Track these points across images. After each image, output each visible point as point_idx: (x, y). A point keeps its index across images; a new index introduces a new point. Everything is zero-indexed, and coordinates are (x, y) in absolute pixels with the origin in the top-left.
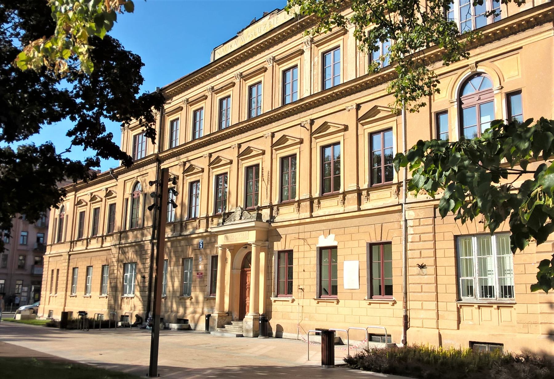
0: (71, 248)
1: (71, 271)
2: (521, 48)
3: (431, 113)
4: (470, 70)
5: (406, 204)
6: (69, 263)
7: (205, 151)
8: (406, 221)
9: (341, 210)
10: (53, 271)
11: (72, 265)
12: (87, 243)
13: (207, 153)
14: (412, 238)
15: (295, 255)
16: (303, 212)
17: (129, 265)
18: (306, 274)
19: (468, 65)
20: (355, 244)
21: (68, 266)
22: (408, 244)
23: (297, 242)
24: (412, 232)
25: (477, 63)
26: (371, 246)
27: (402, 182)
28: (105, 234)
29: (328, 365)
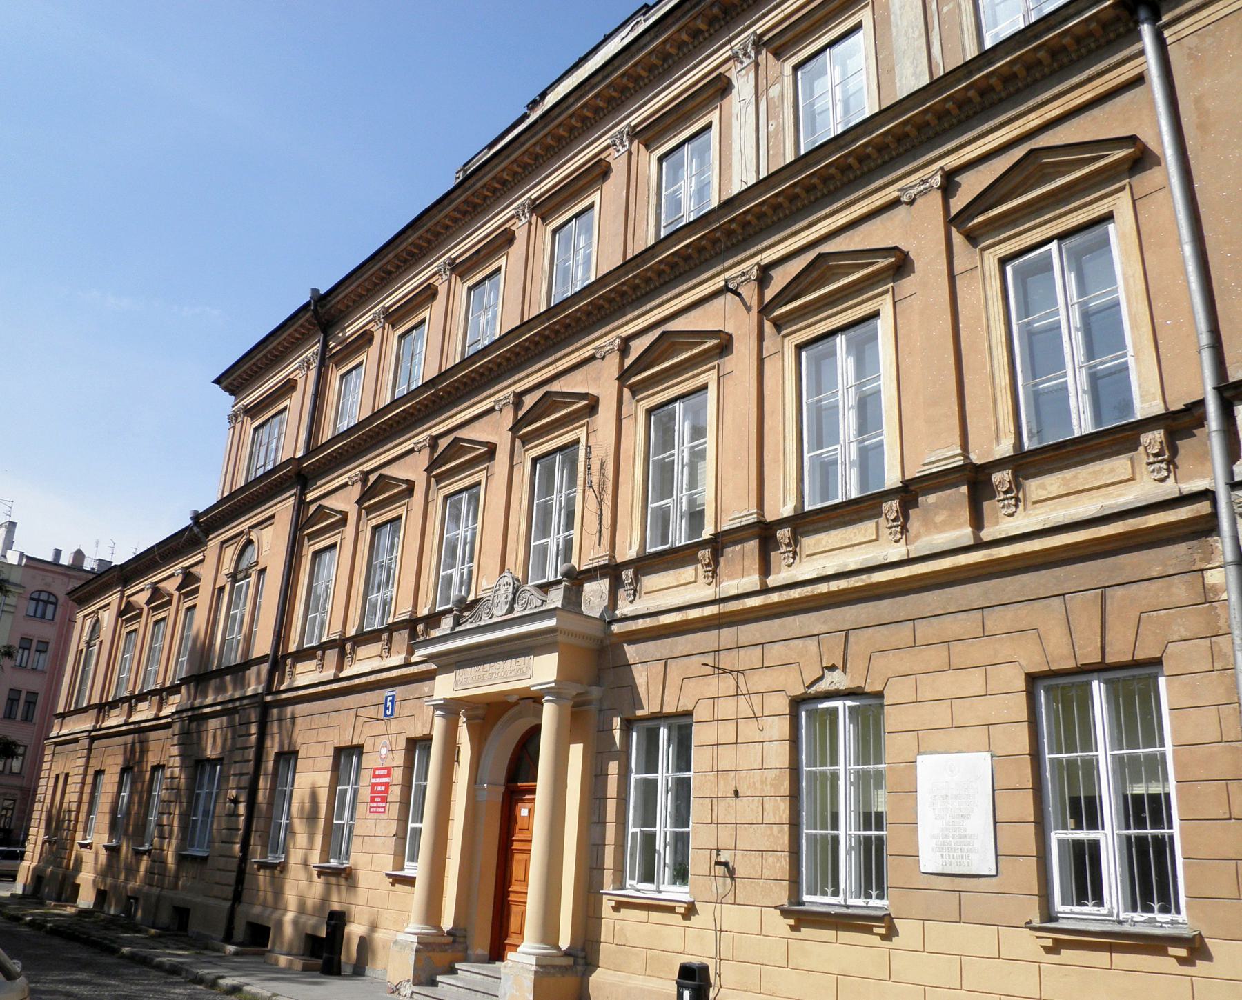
0: (97, 722)
1: (89, 780)
6: (88, 758)
7: (349, 474)
9: (897, 552)
10: (57, 776)
11: (95, 765)
12: (130, 707)
13: (750, 266)
15: (699, 735)
16: (731, 577)
17: (1098, 689)
18: (747, 809)
20: (973, 682)
21: (87, 766)
23: (711, 686)
26: (1032, 679)
28: (351, 632)
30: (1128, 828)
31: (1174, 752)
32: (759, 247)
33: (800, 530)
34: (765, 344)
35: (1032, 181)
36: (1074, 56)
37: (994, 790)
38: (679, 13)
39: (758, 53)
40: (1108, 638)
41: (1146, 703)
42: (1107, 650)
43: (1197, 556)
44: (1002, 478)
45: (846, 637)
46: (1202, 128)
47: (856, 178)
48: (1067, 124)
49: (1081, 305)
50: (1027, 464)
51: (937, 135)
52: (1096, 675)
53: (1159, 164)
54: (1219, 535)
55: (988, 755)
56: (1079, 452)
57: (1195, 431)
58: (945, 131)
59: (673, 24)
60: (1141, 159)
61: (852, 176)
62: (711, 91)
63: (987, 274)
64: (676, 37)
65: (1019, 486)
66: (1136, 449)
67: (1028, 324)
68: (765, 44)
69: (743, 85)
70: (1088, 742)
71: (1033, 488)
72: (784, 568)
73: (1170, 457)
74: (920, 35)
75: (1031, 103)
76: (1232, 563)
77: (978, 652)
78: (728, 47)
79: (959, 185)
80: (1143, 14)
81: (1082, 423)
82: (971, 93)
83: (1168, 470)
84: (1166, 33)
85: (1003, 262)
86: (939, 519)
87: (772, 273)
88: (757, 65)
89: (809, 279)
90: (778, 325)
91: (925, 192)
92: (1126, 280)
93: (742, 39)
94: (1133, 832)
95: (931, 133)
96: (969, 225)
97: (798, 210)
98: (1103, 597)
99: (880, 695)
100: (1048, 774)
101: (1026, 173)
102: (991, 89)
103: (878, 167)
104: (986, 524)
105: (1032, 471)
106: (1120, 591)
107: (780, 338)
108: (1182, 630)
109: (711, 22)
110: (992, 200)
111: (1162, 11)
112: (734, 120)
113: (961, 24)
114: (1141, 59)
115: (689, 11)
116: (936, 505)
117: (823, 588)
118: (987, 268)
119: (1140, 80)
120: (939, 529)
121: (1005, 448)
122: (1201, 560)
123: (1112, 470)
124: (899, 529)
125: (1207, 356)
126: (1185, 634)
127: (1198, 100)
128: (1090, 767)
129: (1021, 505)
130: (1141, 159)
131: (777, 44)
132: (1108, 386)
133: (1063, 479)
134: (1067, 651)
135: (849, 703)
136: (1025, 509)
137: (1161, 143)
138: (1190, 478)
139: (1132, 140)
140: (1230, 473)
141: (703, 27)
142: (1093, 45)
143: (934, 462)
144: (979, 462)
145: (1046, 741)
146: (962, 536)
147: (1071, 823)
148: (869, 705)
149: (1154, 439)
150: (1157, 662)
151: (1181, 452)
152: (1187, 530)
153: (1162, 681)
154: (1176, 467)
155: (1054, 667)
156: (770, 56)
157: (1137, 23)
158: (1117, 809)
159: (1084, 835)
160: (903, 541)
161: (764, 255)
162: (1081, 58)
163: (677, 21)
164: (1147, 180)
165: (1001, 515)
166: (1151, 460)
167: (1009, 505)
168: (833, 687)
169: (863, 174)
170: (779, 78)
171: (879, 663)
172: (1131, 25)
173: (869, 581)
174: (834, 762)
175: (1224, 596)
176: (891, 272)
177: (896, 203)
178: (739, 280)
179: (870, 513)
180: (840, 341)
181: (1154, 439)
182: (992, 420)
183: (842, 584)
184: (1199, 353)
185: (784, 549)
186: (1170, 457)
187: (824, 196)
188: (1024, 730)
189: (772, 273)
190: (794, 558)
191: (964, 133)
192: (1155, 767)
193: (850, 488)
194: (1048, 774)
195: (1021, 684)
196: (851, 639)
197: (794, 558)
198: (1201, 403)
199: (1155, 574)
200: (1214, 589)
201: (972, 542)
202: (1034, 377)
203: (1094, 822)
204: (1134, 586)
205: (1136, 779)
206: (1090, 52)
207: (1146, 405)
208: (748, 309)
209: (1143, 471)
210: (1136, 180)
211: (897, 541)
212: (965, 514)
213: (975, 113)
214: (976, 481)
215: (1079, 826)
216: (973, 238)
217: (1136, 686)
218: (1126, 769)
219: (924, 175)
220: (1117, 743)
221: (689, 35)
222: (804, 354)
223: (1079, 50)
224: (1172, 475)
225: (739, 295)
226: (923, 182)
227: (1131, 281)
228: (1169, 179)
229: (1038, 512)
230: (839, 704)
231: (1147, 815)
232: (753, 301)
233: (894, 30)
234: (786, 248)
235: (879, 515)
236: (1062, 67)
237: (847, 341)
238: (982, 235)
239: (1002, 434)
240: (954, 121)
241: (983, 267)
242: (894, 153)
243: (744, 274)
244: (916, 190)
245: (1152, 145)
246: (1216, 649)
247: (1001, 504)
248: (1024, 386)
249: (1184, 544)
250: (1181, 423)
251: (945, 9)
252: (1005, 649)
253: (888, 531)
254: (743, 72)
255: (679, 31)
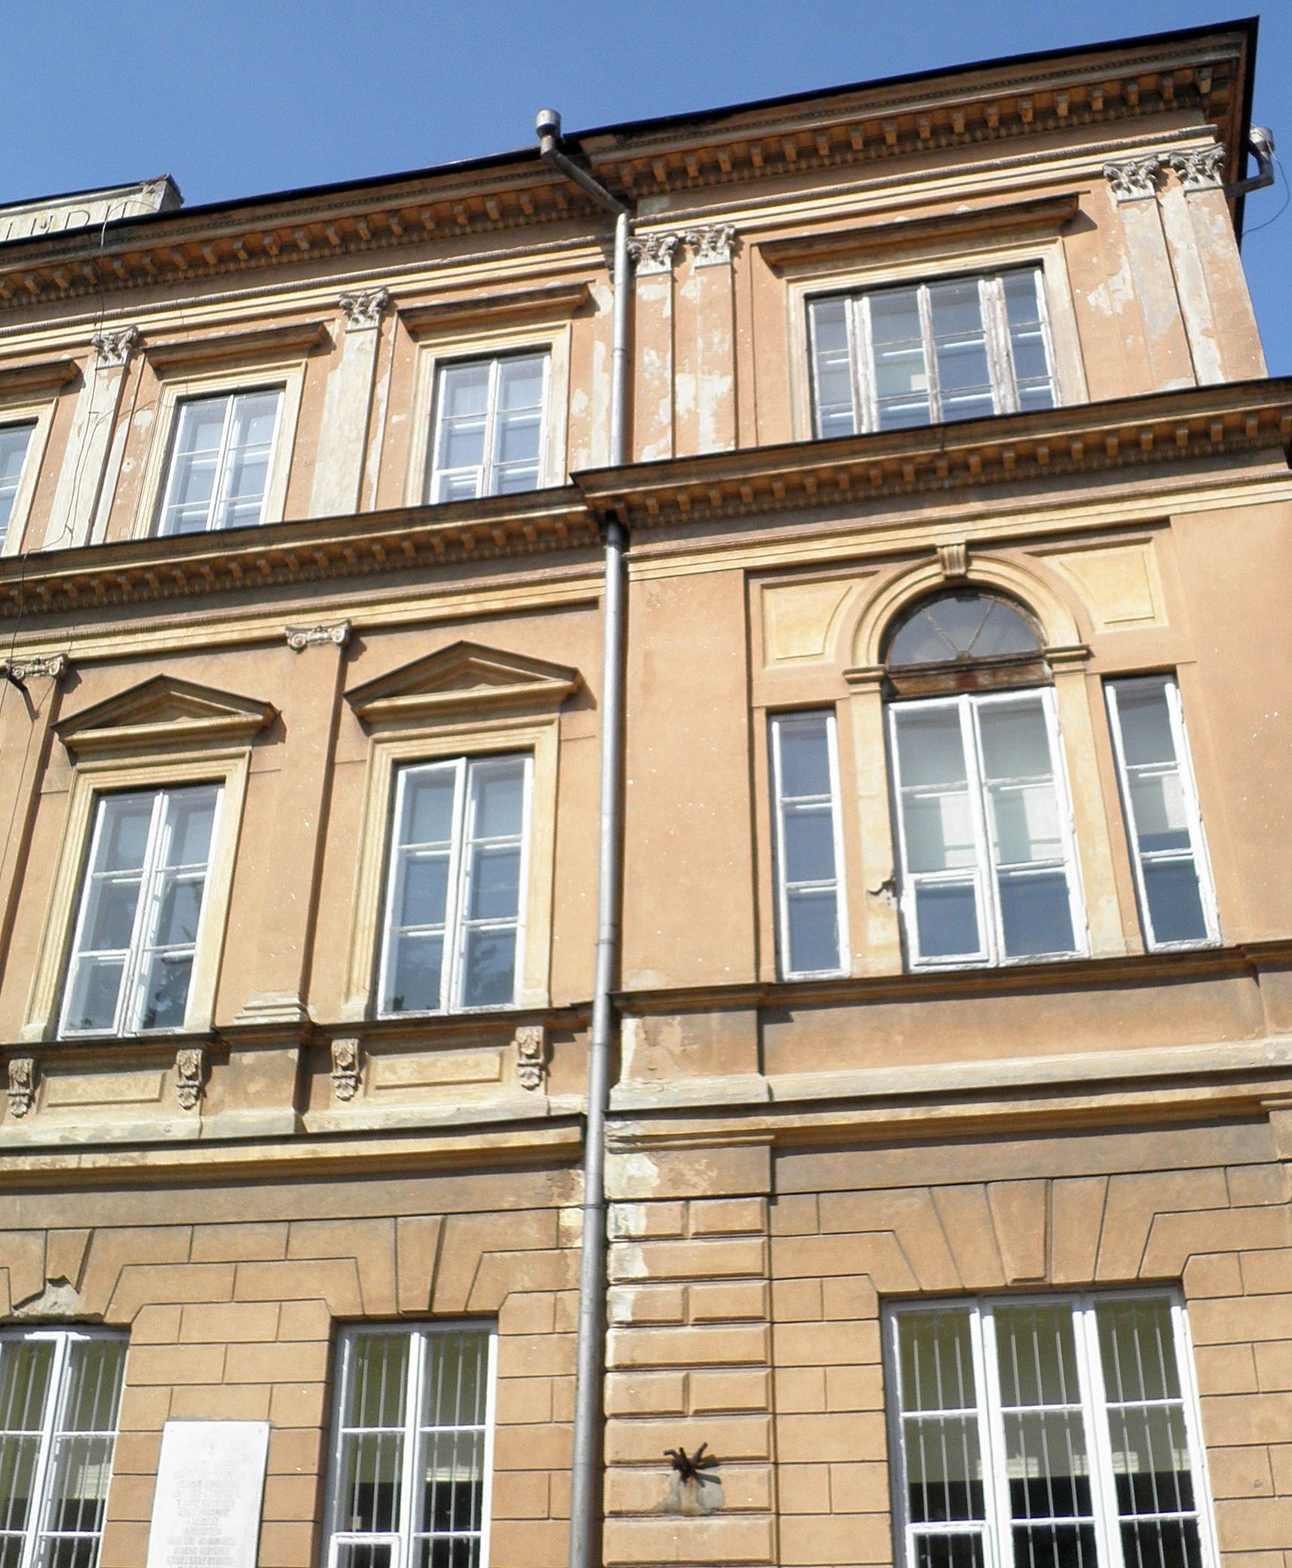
2: (1163, 522)
3: (751, 710)
4: (935, 568)
5: (609, 1115)
8: (603, 1204)
9: (183, 1124)
14: (638, 1304)
17: (417, 1344)
19: (931, 550)
20: (260, 1322)
22: (611, 1334)
24: (640, 1270)
25: (971, 545)
26: (339, 1324)
27: (589, 1006)
29: (104, 886)
30: (426, 1529)
31: (497, 1432)
32: (71, 631)
33: (46, 1065)
34: (48, 773)
35: (453, 677)
36: (531, 548)
37: (266, 1475)
38: (33, 249)
39: (132, 355)
40: (440, 1280)
41: (470, 1366)
42: (437, 1295)
43: (556, 1190)
44: (344, 1048)
45: (91, 1238)
46: (646, 687)
47: (233, 589)
48: (505, 622)
49: (476, 845)
50: (376, 1036)
51: (350, 575)
52: (417, 1325)
53: (594, 707)
54: (583, 1168)
55: (265, 1426)
56: (444, 1034)
57: (576, 1035)
58: (361, 575)
59: (19, 259)
60: (575, 697)
61: (228, 585)
62: (49, 377)
63: (375, 775)
64: (15, 276)
65: (363, 1062)
66: (508, 1043)
67: (409, 851)
68: (150, 352)
69: (99, 389)
70: (394, 1414)
71: (380, 1069)
72: (9, 1118)
73: (544, 1061)
74: (357, 439)
75: (473, 582)
76: (593, 1206)
77: (276, 1280)
78: (91, 327)
79: (364, 648)
80: (612, 534)
81: (451, 1001)
82: (406, 544)
83: (540, 1077)
84: (631, 567)
85: (398, 764)
86: (253, 1088)
87: (82, 673)
88: (127, 372)
89: (137, 704)
90: (74, 753)
91: (321, 643)
92: (533, 832)
93: (117, 327)
94: (433, 1535)
95: (345, 571)
96: (370, 707)
97: (141, 601)
98: (443, 1225)
99: (125, 1329)
100: (339, 1455)
101: (448, 666)
102: (430, 547)
103: (266, 586)
104: (312, 1104)
105: (383, 1045)
106: (463, 1222)
107: (73, 771)
108: (526, 1278)
109: (75, 281)
110: (401, 686)
111: (632, 540)
112: (73, 432)
113: (410, 447)
114: (600, 582)
115: (48, 254)
116: (253, 1069)
117: (71, 1161)
118: (376, 766)
119: (592, 604)
120: (251, 1102)
121: (353, 1011)
122: (560, 1195)
123: (477, 1065)
124: (194, 1091)
125: (604, 953)
126: (529, 1285)
127: (647, 656)
128: (393, 1446)
129: (361, 1087)
130: (575, 697)
131: (164, 358)
132: (489, 961)
133: (419, 1064)
134: (387, 1291)
135: (74, 1336)
136: (365, 1093)
137: (602, 687)
138: (561, 1090)
139: (572, 673)
140: (606, 1099)
141: (62, 283)
142: (553, 544)
143: (260, 1008)
144: (315, 1020)
145: (342, 1409)
146: (280, 1119)
147: (357, 1521)
148: (105, 1343)
149: (530, 1035)
150: (492, 1317)
151: (557, 1056)
152: (549, 1156)
153: (493, 1340)
154: (548, 1074)
155: (369, 1312)
156: (149, 369)
157: (604, 540)
158: (418, 1506)
159: (372, 1539)
160: (196, 1109)
161: (75, 645)
162: (537, 553)
163: (26, 258)
164: (580, 721)
165: (334, 1097)
166: (524, 1061)
167: (347, 1086)
168: (56, 1311)
169: (244, 588)
170: (154, 404)
171: (133, 1281)
172: (598, 539)
173: (141, 1162)
174: (35, 1423)
175: (578, 1243)
176: (253, 732)
177: (279, 641)
178: (29, 668)
179: (158, 1060)
180: (161, 802)
181: (530, 1035)
182: (345, 968)
183: (102, 1160)
184: (597, 945)
185: (15, 1089)
186: (544, 1061)
187: (182, 595)
188: (319, 1392)
189: (82, 673)
190: (28, 1106)
191: (385, 586)
192: (470, 1449)
193: (128, 1020)
194: (339, 1455)
195: (323, 1331)
196: (97, 1242)
197: (28, 1106)
198: (589, 1006)
199: (506, 1206)
200: (568, 1234)
201: (290, 1131)
202: (403, 924)
203: (386, 1523)
204: (481, 1217)
205: (445, 1462)
206: (549, 550)
207: (528, 994)
208: (34, 715)
209: (512, 1071)
210: (568, 717)
211: (187, 1108)
212: (289, 1088)
213: (404, 568)
214: (312, 1044)
215: (366, 1527)
216: (367, 723)
217: (462, 1344)
218: (435, 1450)
219: (324, 619)
220: (429, 1418)
221: (37, 284)
222: (103, 805)
223: (538, 543)
224: (543, 1084)
225: (24, 689)
226: (321, 629)
227: (539, 836)
228: (601, 728)
229: (381, 1101)
230: (60, 1338)
231: (452, 1513)
232: (45, 707)
233: (325, 415)
234: (118, 652)
235: (170, 1065)
236: (514, 555)
237: (171, 801)
238: (379, 722)
239: (354, 989)
240: (377, 567)
241: (373, 763)
242: (291, 577)
243: (39, 662)
244: (309, 636)
245: (591, 683)
246: (560, 1307)
247: (337, 1083)
248: (392, 932)
249: (544, 1173)
250: (563, 1023)
251: (395, 419)
252: (311, 1280)
253: (179, 1091)
254: (105, 372)
255: (25, 272)
